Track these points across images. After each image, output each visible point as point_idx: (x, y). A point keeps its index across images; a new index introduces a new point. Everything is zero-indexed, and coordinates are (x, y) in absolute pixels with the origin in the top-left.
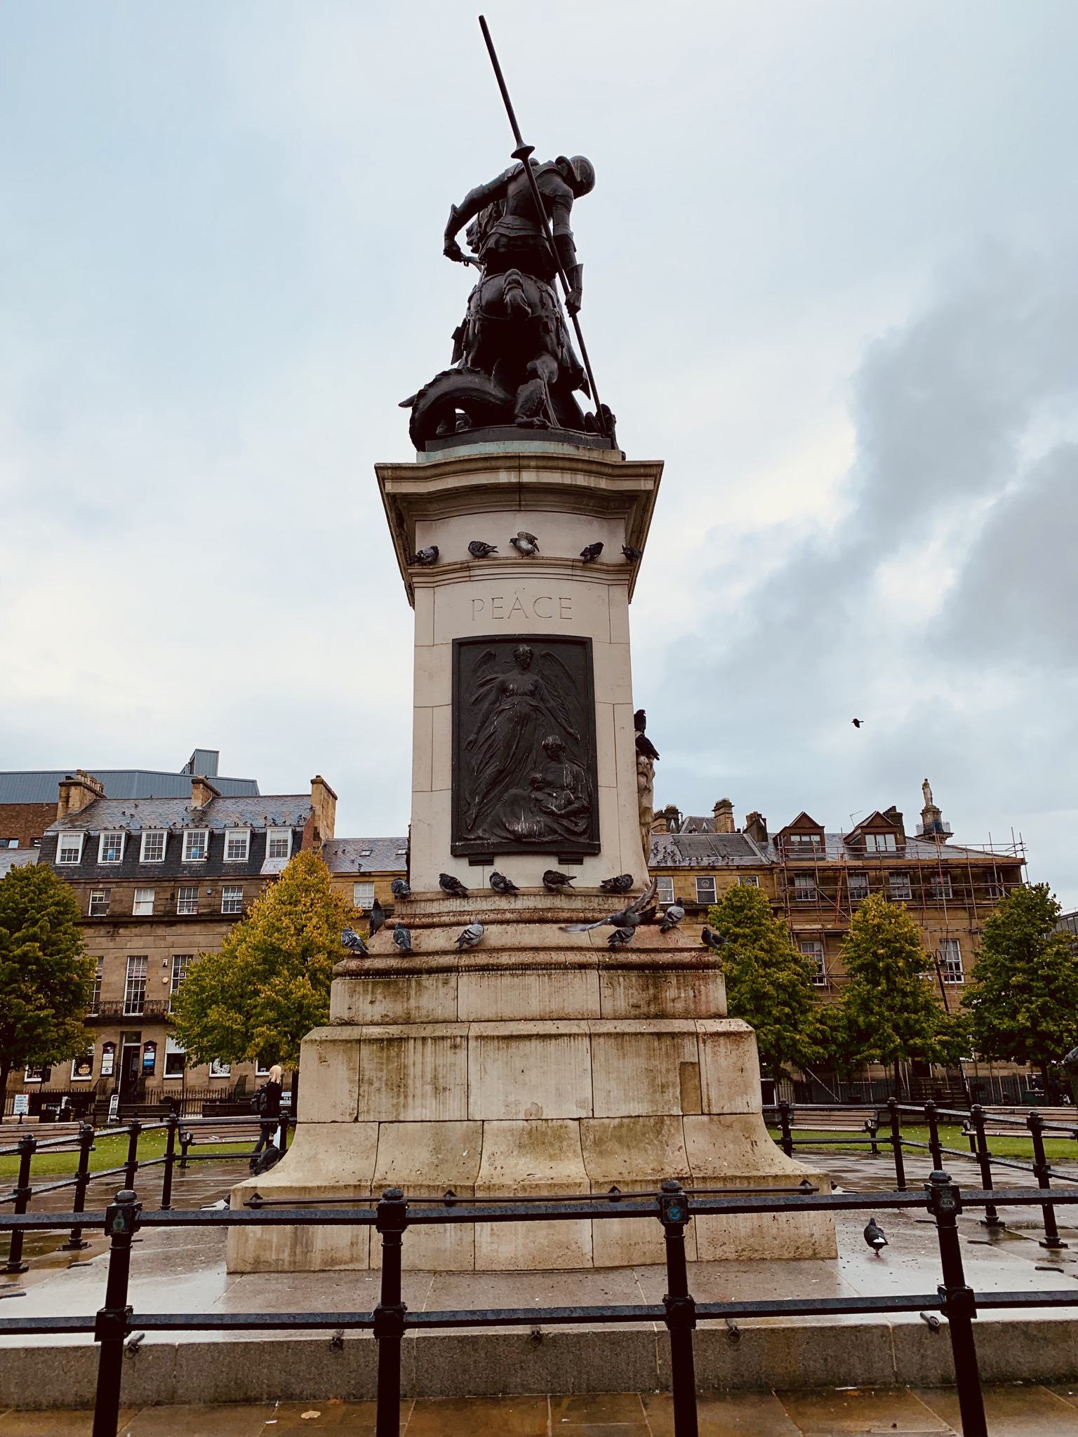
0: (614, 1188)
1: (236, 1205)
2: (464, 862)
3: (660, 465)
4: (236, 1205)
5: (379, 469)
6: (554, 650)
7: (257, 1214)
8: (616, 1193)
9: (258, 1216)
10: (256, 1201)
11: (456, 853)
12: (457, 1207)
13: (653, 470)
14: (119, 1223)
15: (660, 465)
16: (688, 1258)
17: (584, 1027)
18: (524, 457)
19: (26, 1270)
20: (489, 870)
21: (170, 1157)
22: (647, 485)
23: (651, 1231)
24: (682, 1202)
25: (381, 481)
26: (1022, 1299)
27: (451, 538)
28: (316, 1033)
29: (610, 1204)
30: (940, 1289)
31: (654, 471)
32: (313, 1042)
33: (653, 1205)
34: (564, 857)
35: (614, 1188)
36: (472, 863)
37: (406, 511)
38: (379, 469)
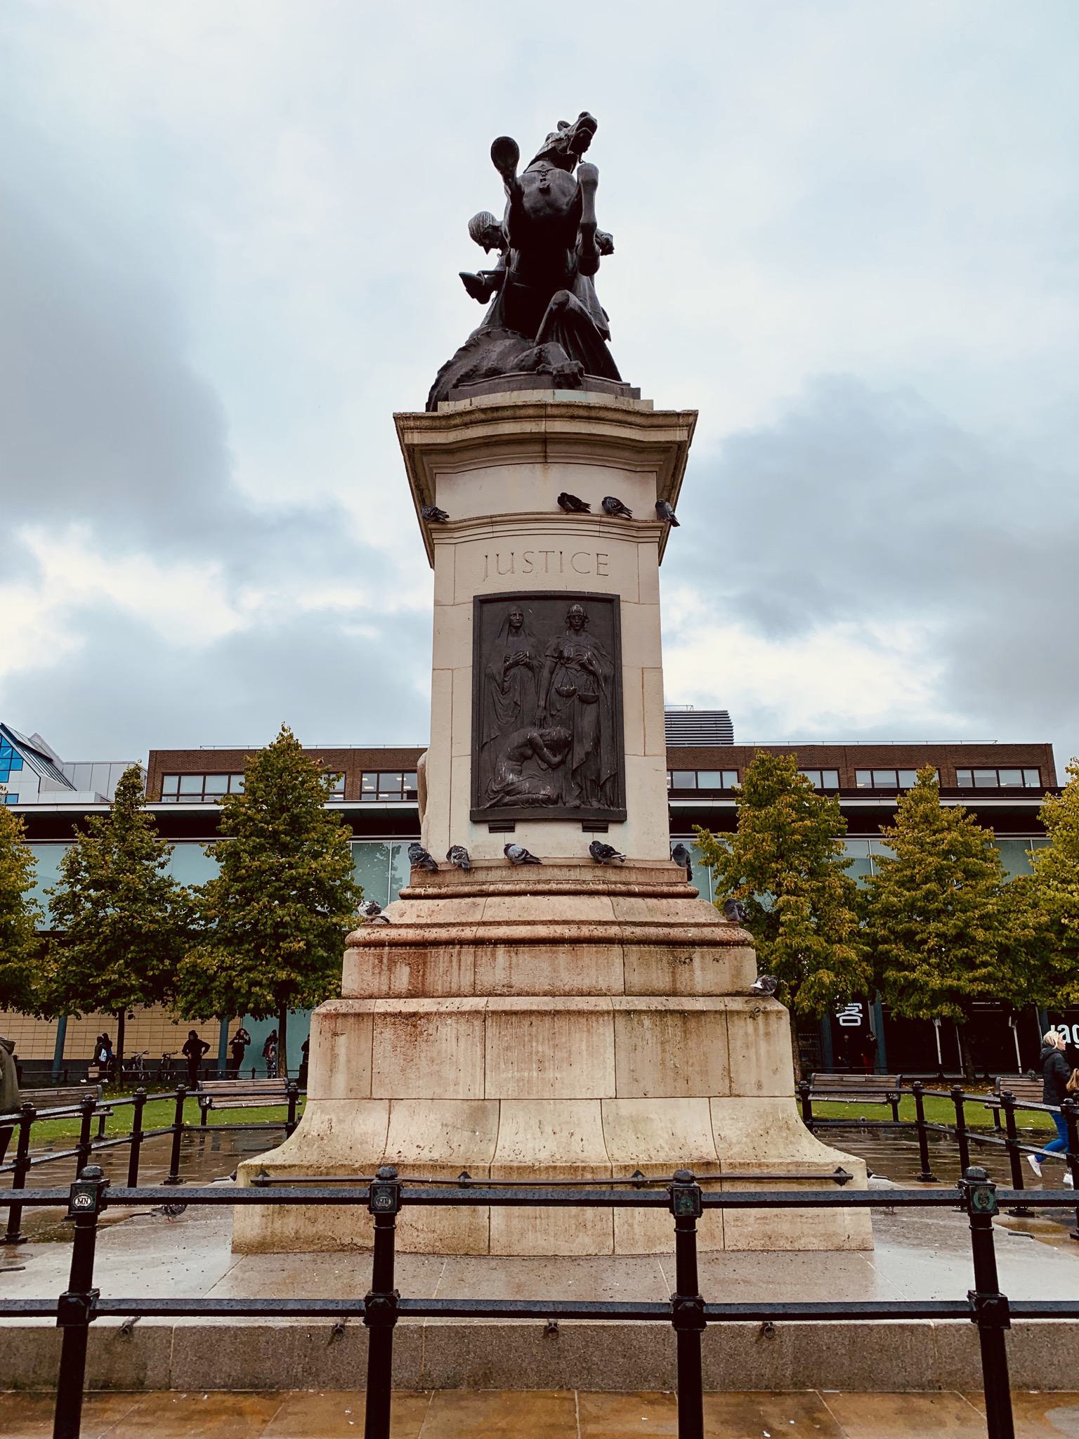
0: (465, 1175)
1: (242, 1182)
2: (484, 829)
3: (694, 414)
4: (242, 1182)
5: (397, 418)
6: (531, 608)
7: (641, 1194)
8: (640, 1178)
9: (508, 1196)
10: (262, 1179)
11: (476, 819)
12: (465, 1191)
13: (688, 420)
14: (384, 1201)
15: (694, 414)
16: (396, 1249)
17: (656, 1003)
18: (594, 408)
19: (24, 1241)
20: (502, 838)
21: (179, 1128)
22: (679, 435)
23: (663, 1221)
24: (695, 1193)
25: (401, 431)
26: (159, 1306)
27: (456, 498)
28: (331, 1005)
29: (634, 1190)
30: (970, 1295)
31: (691, 419)
32: (318, 1014)
33: (361, 1191)
34: (492, 825)
35: (637, 1174)
36: (492, 830)
37: (424, 466)
38: (397, 418)
